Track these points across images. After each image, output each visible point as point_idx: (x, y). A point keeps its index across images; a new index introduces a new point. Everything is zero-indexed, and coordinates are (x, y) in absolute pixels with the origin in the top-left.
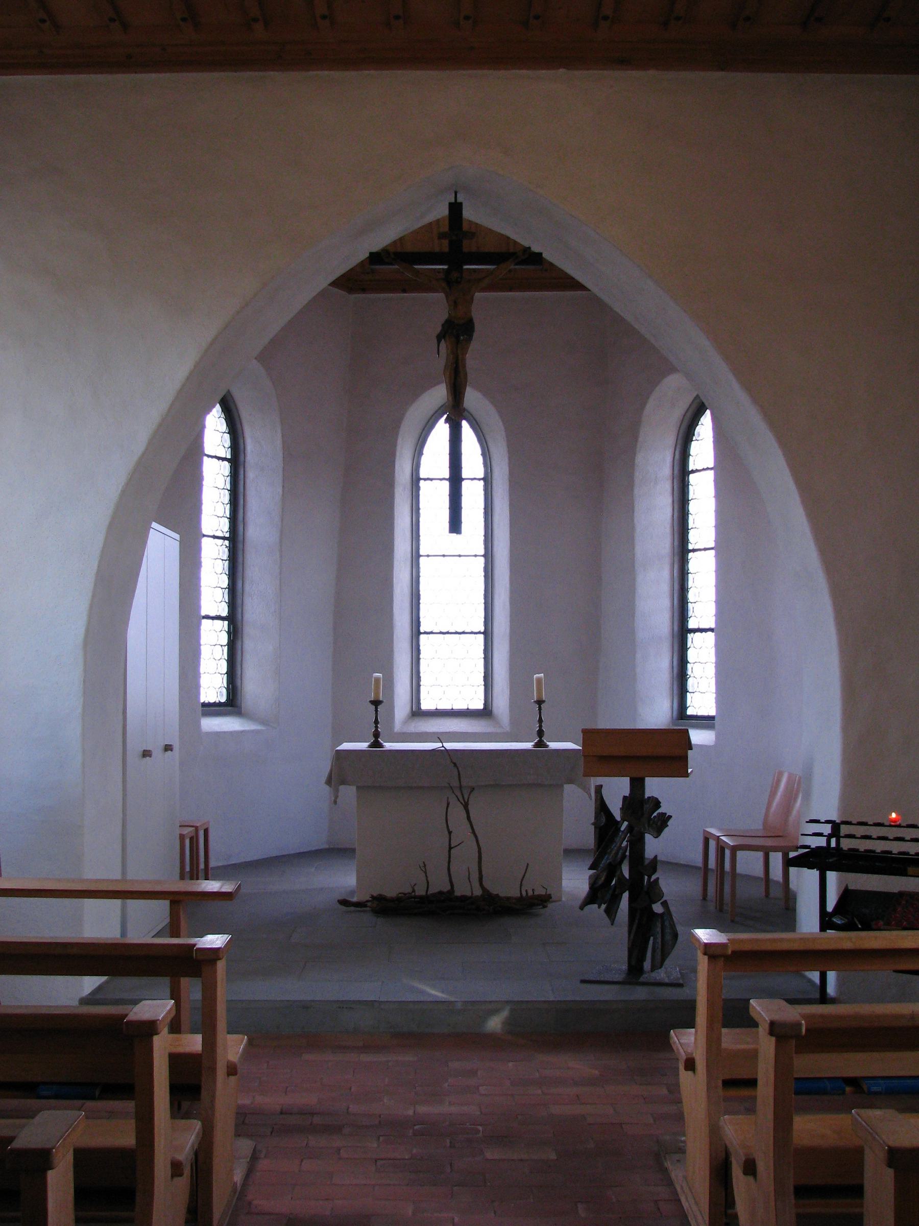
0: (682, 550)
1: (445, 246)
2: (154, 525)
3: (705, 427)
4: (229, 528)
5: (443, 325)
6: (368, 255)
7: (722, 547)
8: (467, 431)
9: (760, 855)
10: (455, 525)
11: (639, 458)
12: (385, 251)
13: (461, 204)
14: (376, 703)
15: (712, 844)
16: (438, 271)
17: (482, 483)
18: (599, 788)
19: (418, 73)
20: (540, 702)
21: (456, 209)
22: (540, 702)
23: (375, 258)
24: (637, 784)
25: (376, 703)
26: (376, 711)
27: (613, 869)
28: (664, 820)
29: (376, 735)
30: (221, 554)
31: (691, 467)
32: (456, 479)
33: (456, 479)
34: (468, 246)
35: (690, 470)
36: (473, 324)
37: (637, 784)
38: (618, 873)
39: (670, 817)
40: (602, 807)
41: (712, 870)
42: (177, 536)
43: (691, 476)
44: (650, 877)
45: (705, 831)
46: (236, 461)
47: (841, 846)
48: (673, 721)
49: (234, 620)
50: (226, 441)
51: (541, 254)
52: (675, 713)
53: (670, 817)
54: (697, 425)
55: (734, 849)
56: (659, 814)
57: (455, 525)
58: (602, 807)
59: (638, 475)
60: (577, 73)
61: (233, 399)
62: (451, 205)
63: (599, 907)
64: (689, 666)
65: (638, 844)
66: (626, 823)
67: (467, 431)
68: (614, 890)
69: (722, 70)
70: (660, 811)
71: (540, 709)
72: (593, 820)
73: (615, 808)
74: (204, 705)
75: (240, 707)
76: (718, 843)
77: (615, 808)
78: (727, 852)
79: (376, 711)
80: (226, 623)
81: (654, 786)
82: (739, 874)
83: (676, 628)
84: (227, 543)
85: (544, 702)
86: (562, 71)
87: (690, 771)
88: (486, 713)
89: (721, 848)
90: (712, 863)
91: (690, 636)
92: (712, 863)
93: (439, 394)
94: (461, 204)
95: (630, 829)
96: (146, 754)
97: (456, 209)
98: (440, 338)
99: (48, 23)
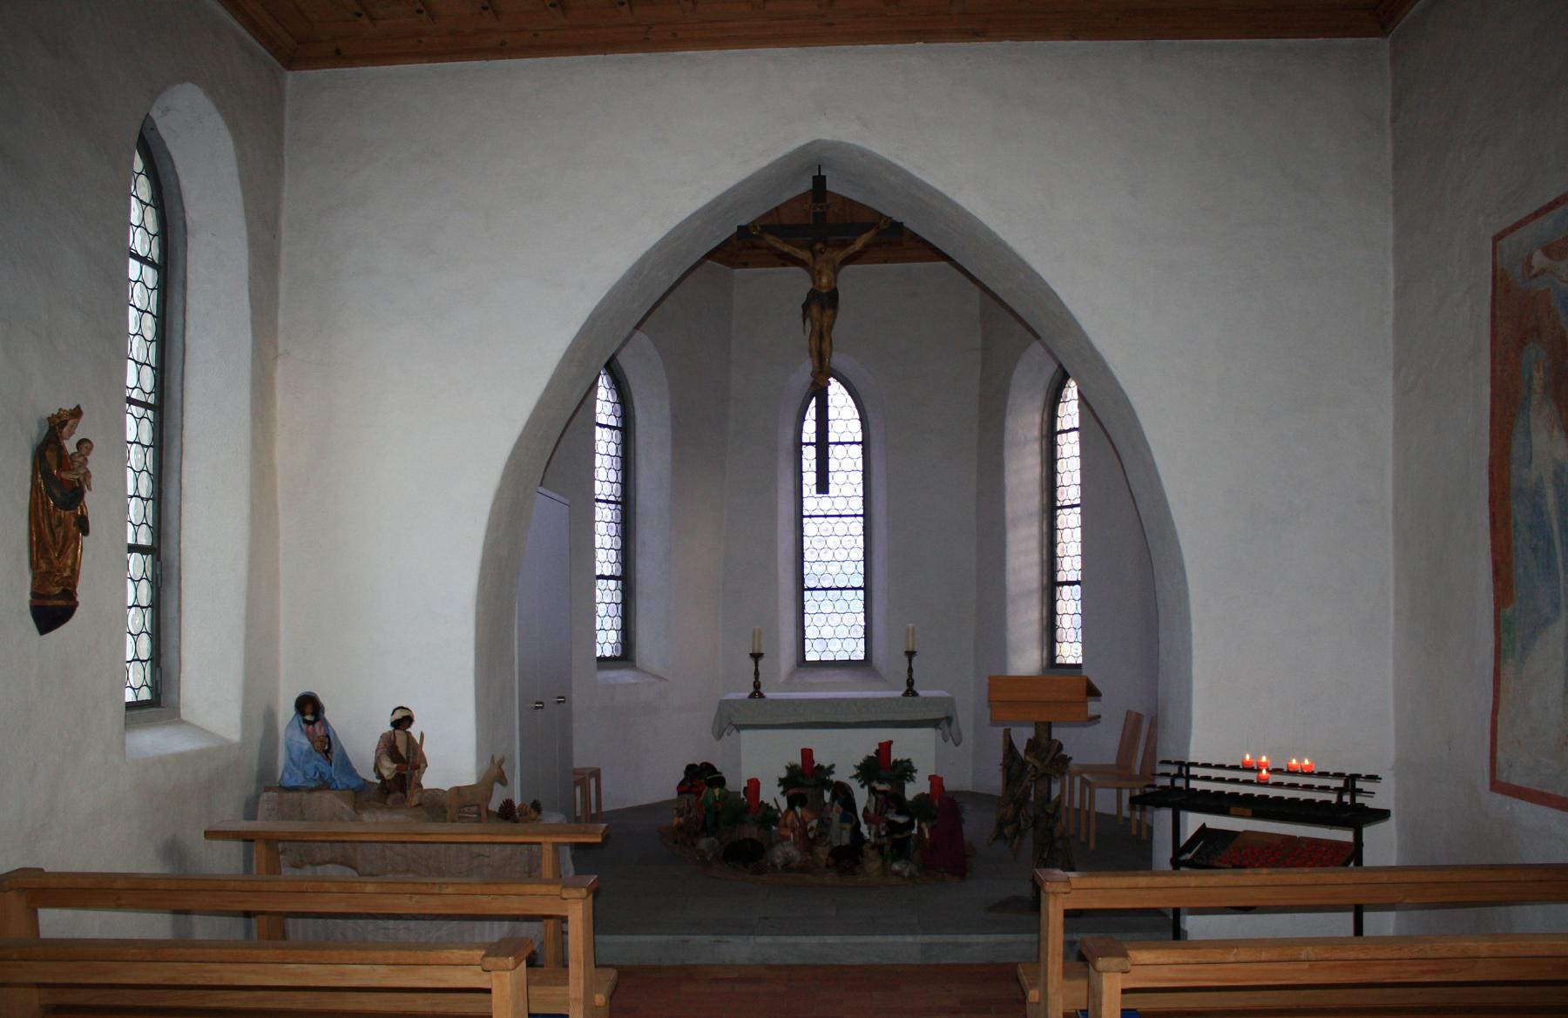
0: (1051, 507)
3: (1071, 391)
6: (735, 229)
7: (1087, 505)
8: (837, 394)
11: (1009, 423)
14: (757, 657)
17: (860, 447)
19: (780, 50)
21: (819, 181)
25: (757, 657)
29: (910, 683)
30: (614, 517)
31: (1059, 428)
33: (822, 444)
35: (1058, 430)
36: (837, 295)
40: (1010, 747)
46: (626, 429)
47: (785, 798)
48: (1043, 670)
49: (626, 579)
50: (616, 411)
51: (902, 223)
52: (1045, 663)
58: (1010, 747)
59: (1008, 438)
60: (932, 45)
61: (1052, 380)
62: (814, 177)
64: (1058, 618)
67: (837, 394)
69: (1074, 39)
72: (1001, 761)
73: (1021, 747)
74: (602, 659)
75: (635, 662)
77: (1021, 747)
80: (620, 582)
83: (1045, 582)
84: (619, 507)
86: (919, 44)
93: (807, 368)
94: (825, 176)
97: (819, 181)
99: (425, 13)
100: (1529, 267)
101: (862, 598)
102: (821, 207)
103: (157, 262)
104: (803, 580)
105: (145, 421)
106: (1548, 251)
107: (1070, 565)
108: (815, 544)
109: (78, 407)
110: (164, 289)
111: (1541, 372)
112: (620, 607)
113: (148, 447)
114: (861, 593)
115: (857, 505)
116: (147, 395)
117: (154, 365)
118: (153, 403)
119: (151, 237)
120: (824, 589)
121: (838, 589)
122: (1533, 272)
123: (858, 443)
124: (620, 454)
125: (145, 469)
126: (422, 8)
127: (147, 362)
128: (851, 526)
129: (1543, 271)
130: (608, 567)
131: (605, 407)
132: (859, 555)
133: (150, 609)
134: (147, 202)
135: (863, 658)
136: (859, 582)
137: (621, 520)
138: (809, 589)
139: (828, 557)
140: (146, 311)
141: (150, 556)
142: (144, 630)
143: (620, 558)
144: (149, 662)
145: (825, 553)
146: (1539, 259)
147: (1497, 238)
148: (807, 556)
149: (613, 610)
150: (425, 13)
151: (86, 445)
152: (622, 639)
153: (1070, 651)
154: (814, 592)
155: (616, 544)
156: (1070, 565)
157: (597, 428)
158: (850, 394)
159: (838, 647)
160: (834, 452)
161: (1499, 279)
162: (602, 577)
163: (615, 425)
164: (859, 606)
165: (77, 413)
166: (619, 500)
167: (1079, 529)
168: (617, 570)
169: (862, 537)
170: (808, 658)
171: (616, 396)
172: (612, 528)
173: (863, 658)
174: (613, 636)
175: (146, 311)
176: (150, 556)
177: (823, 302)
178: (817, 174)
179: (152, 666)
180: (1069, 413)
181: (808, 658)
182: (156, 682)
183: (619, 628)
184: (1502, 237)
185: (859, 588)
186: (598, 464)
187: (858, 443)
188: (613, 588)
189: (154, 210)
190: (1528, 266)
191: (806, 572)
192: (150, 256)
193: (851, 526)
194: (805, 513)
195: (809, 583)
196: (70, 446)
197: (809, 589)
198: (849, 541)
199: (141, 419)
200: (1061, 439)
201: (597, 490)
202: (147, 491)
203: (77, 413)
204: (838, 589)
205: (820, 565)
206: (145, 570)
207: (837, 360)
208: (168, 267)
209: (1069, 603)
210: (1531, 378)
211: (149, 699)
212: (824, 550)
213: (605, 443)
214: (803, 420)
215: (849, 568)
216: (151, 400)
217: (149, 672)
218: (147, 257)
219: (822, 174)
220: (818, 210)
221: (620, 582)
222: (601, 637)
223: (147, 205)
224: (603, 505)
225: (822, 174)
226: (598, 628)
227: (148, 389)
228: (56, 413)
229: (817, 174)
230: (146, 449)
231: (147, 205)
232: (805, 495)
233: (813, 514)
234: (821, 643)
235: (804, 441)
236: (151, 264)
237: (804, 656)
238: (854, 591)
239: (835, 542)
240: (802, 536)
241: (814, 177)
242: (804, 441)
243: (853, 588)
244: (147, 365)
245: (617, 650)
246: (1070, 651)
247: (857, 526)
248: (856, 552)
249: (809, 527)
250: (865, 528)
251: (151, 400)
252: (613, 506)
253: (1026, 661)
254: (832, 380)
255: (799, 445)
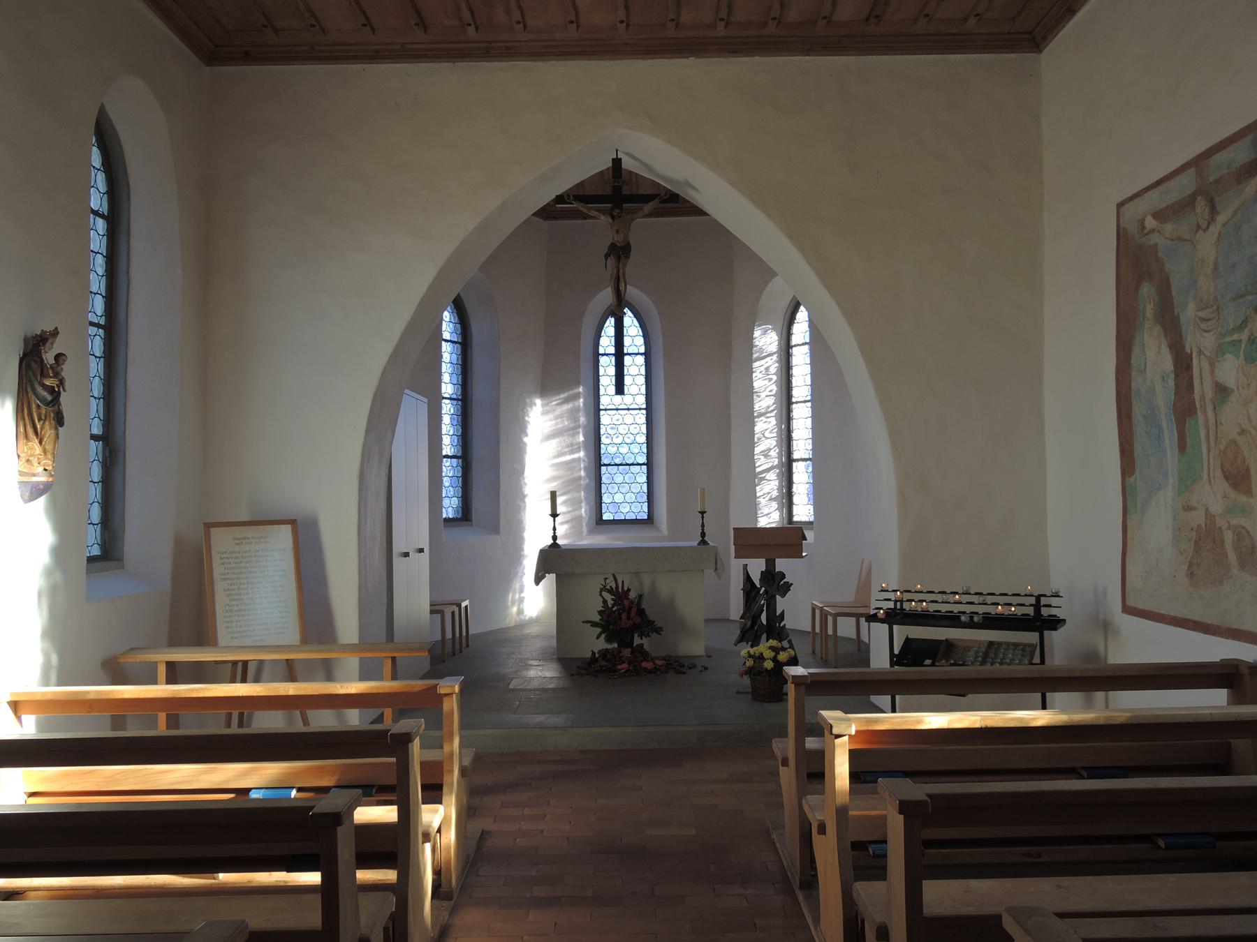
1: (608, 191)
2: (407, 391)
3: (802, 315)
4: (105, 310)
5: (609, 248)
8: (629, 320)
9: (853, 619)
10: (620, 389)
12: (567, 193)
13: (621, 159)
15: (818, 612)
16: (608, 207)
18: (745, 566)
20: (702, 513)
22: (702, 513)
23: (559, 199)
24: (770, 563)
26: (554, 521)
27: (756, 618)
28: (788, 587)
32: (619, 355)
33: (619, 355)
34: (626, 190)
37: (770, 563)
38: (759, 622)
39: (792, 584)
40: (748, 578)
41: (818, 634)
42: (426, 400)
43: (794, 349)
44: (780, 624)
45: (812, 603)
49: (435, 457)
50: (458, 329)
53: (792, 584)
54: (798, 312)
55: (836, 616)
56: (784, 582)
57: (620, 389)
58: (748, 578)
62: (613, 159)
63: (747, 644)
65: (771, 605)
66: (763, 589)
67: (629, 320)
68: (757, 632)
70: (785, 580)
71: (703, 517)
74: (447, 520)
76: (821, 613)
77: (756, 579)
78: (830, 619)
79: (554, 521)
80: (460, 460)
81: (781, 565)
82: (839, 637)
84: (460, 403)
85: (705, 512)
87: (804, 554)
88: (650, 520)
89: (824, 616)
90: (818, 630)
91: (795, 464)
92: (818, 630)
93: (606, 296)
94: (621, 159)
95: (766, 592)
96: (406, 555)
98: (607, 256)
99: (317, 27)
100: (1144, 228)
101: (646, 472)
102: (618, 182)
103: (106, 214)
104: (600, 458)
105: (98, 337)
106: (1158, 215)
107: (802, 445)
108: (610, 431)
109: (56, 328)
110: (113, 235)
111: (1152, 305)
112: (460, 479)
113: (100, 358)
114: (644, 467)
115: (641, 401)
116: (99, 318)
117: (104, 294)
118: (103, 324)
119: (102, 195)
120: (616, 465)
121: (627, 464)
122: (1146, 231)
123: (641, 354)
124: (460, 363)
125: (97, 375)
126: (315, 23)
127: (99, 292)
128: (637, 417)
129: (1153, 231)
130: (451, 449)
131: (448, 328)
132: (642, 439)
133: (100, 484)
134: (98, 168)
135: (646, 518)
136: (642, 459)
137: (462, 413)
138: (605, 465)
139: (619, 440)
140: (98, 253)
141: (101, 442)
142: (96, 500)
143: (460, 441)
144: (100, 525)
145: (617, 437)
146: (1150, 223)
147: (1120, 205)
148: (603, 439)
149: (455, 482)
150: (317, 27)
151: (63, 357)
152: (462, 505)
153: (803, 511)
154: (609, 467)
155: (458, 431)
156: (802, 445)
157: (443, 342)
158: (635, 316)
159: (628, 509)
160: (627, 360)
161: (1121, 234)
162: (447, 456)
163: (456, 340)
164: (643, 478)
165: (55, 333)
166: (460, 397)
167: (810, 419)
168: (458, 451)
169: (645, 425)
170: (605, 517)
171: (457, 318)
172: (454, 419)
173: (646, 518)
174: (455, 502)
175: (98, 253)
176: (101, 442)
177: (620, 252)
178: (615, 157)
179: (101, 527)
180: (801, 330)
181: (605, 517)
182: (105, 540)
183: (460, 495)
184: (1124, 205)
185: (603, 355)
186: (443, 370)
187: (641, 354)
188: (455, 465)
189: (103, 174)
190: (1142, 222)
191: (602, 452)
192: (101, 210)
193: (637, 417)
194: (601, 407)
195: (605, 461)
196: (49, 358)
197: (605, 465)
198: (635, 428)
199: (94, 336)
200: (795, 351)
201: (443, 391)
202: (99, 391)
203: (55, 333)
204: (627, 464)
205: (613, 447)
206: (97, 454)
207: (632, 292)
208: (115, 218)
209: (802, 475)
210: (1144, 308)
211: (99, 554)
212: (615, 436)
213: (448, 353)
214: (598, 336)
215: (635, 449)
216: (102, 322)
217: (99, 533)
218: (98, 210)
219: (619, 157)
220: (616, 184)
221: (460, 460)
222: (446, 502)
223: (98, 170)
224: (448, 401)
225: (619, 157)
226: (444, 496)
227: (99, 314)
228: (38, 333)
229: (615, 157)
230: (98, 359)
231: (98, 170)
232: (601, 393)
233: (608, 407)
234: (614, 506)
235: (645, 467)
236: (102, 216)
237: (602, 516)
238: (639, 467)
239: (624, 429)
240: (599, 425)
241: (613, 159)
242: (645, 467)
243: (638, 464)
244: (99, 294)
245: (458, 512)
246: (803, 511)
247: (641, 418)
248: (640, 476)
249: (605, 418)
250: (647, 419)
251: (102, 322)
252: (455, 402)
253: (769, 517)
254: (626, 310)
255: (597, 355)
